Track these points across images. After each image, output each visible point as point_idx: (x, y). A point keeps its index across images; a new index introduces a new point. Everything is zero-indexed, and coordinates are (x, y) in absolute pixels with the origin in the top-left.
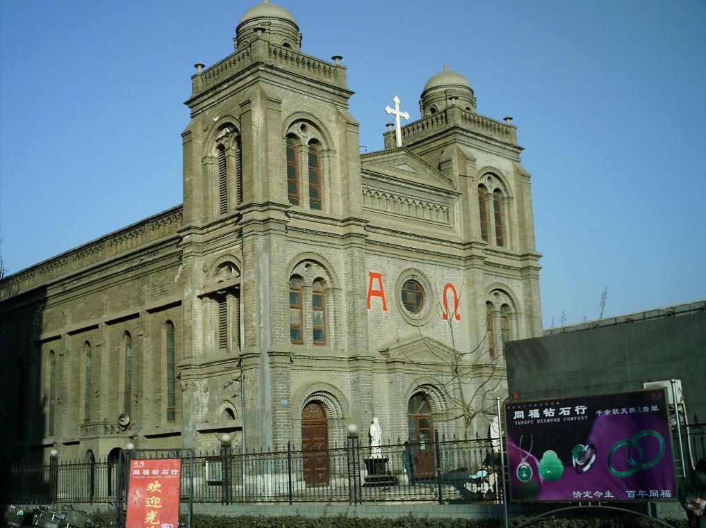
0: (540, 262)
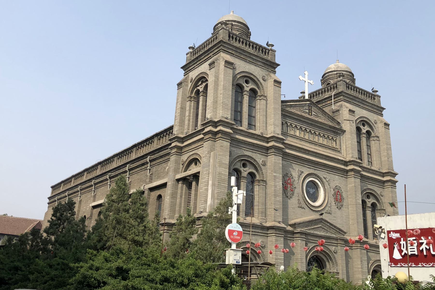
0: (396, 178)
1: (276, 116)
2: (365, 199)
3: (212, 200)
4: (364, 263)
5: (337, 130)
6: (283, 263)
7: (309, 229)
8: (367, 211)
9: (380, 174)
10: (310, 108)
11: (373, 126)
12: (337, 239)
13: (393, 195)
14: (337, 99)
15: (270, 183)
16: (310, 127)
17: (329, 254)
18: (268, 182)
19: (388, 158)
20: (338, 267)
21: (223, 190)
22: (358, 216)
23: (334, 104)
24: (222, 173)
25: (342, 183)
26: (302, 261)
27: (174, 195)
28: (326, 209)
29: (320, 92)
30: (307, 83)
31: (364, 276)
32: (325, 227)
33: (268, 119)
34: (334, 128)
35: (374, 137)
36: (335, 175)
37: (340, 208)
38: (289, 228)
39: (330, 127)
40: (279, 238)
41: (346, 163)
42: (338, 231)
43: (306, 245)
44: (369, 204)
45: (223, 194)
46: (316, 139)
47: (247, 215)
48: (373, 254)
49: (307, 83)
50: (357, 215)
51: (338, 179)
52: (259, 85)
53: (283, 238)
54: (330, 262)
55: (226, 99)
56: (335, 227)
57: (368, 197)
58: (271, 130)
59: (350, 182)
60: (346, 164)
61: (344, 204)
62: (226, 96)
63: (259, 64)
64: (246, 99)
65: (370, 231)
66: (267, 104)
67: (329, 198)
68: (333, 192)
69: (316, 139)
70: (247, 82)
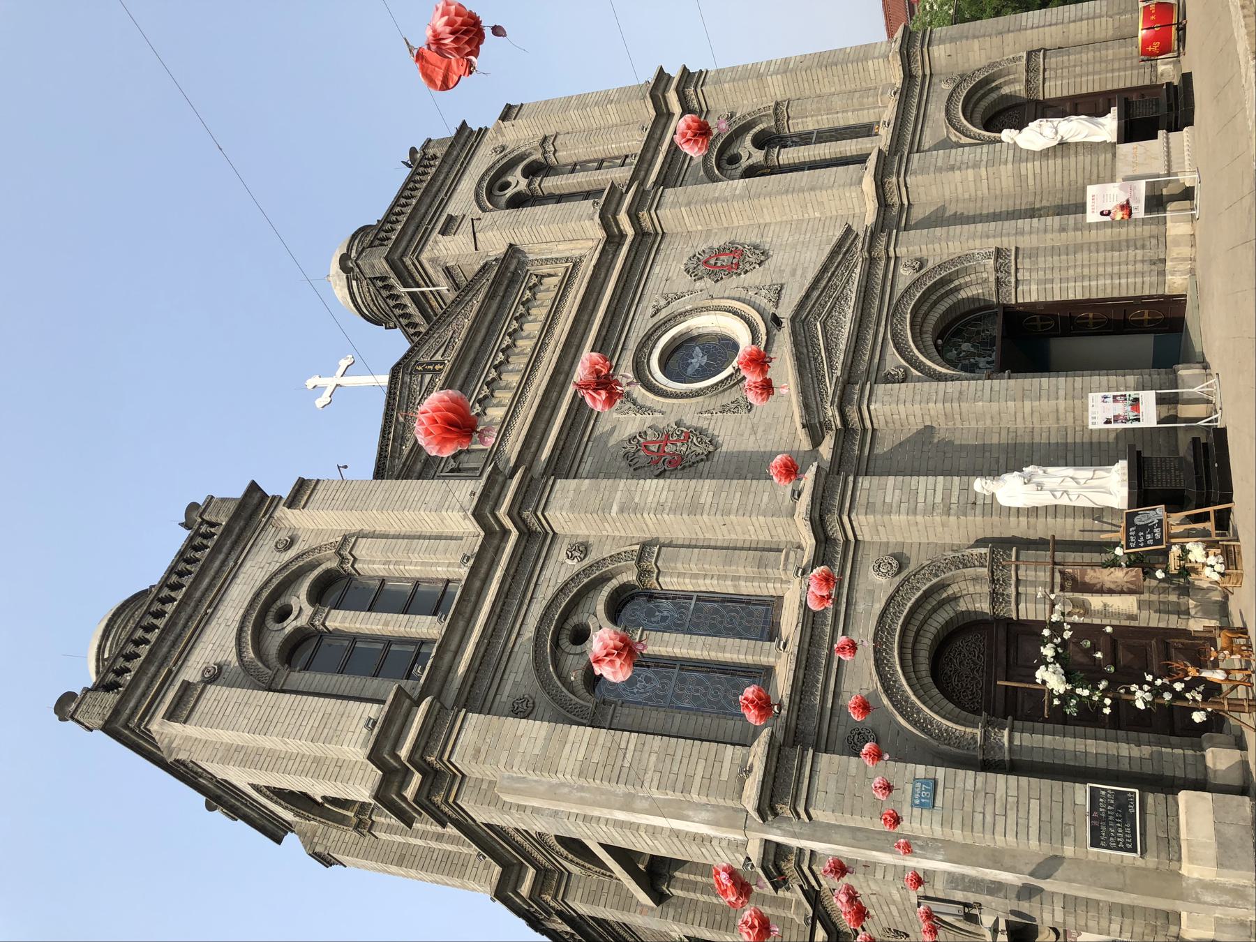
0: (674, 72)
1: (411, 500)
2: (740, 171)
3: (691, 813)
4: (959, 158)
5: (503, 274)
6: (965, 478)
7: (831, 367)
8: (781, 162)
9: (660, 126)
10: (420, 368)
11: (511, 156)
12: (871, 262)
13: (728, 78)
14: (418, 277)
15: (650, 526)
16: (482, 366)
17: (925, 288)
18: (647, 536)
19: (611, 102)
20: (976, 251)
21: (654, 757)
22: (791, 189)
23: (434, 286)
24: (580, 757)
25: (679, 250)
26: (956, 395)
27: (718, 917)
28: (763, 305)
29: (412, 331)
30: (348, 381)
31: (1004, 157)
32: (824, 308)
33: (427, 530)
34: (496, 282)
35: (545, 152)
36: (651, 276)
37: (763, 255)
38: (826, 449)
39: (490, 296)
40: (861, 497)
41: (613, 239)
42: (841, 256)
43: (889, 379)
44: (758, 156)
45: (668, 759)
46: (525, 345)
47: (771, 633)
48: (927, 132)
49: (348, 381)
50: (787, 192)
51: (665, 263)
52: (301, 564)
53: (860, 479)
54: (956, 283)
55: (304, 723)
56: (824, 269)
57: (735, 159)
58: (461, 520)
59: (677, 223)
60: (617, 240)
61: (754, 238)
62: (293, 721)
63: (231, 564)
64: (339, 620)
65: (848, 148)
66: (373, 535)
67: (726, 295)
68: (708, 282)
69: (525, 345)
70: (284, 614)
